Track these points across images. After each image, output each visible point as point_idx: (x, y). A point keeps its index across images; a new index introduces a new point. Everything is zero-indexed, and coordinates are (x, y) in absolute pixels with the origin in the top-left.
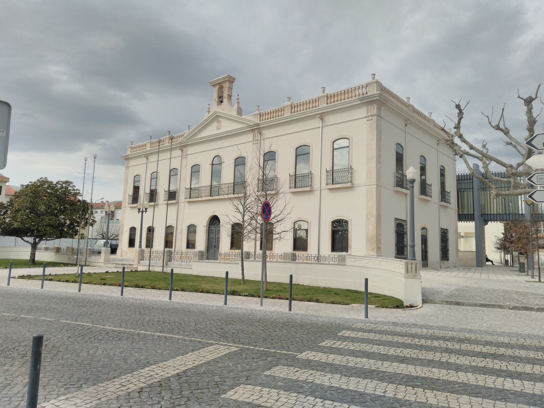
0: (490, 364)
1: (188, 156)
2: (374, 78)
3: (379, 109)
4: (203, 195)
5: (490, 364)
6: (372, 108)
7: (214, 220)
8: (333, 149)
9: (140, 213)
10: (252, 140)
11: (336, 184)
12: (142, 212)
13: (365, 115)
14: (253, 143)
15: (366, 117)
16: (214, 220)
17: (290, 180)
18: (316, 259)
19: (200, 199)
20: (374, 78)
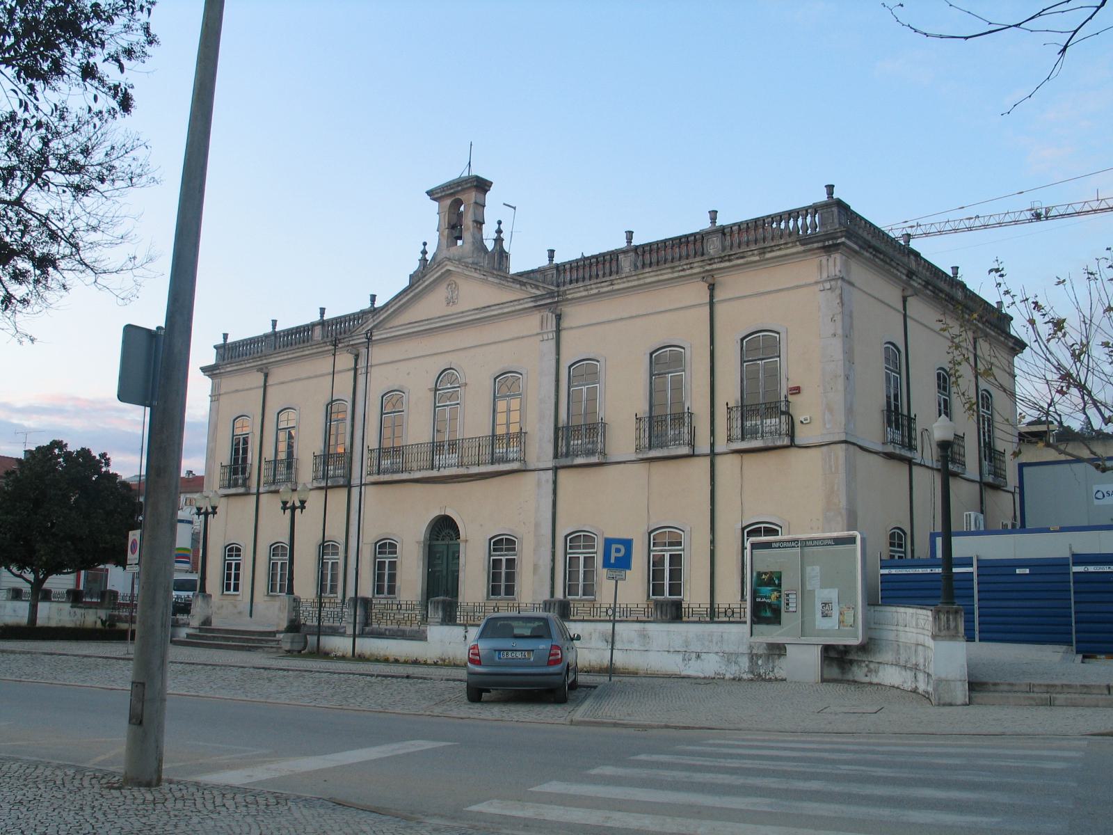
0: (855, 789)
1: (221, 397)
2: (713, 220)
3: (846, 265)
4: (415, 466)
5: (855, 789)
6: (831, 260)
7: (444, 528)
8: (278, 429)
9: (288, 512)
10: (539, 331)
11: (384, 473)
12: (293, 509)
13: (816, 277)
14: (540, 337)
15: (817, 283)
16: (444, 528)
17: (638, 429)
18: (610, 612)
19: (405, 476)
20: (713, 220)
